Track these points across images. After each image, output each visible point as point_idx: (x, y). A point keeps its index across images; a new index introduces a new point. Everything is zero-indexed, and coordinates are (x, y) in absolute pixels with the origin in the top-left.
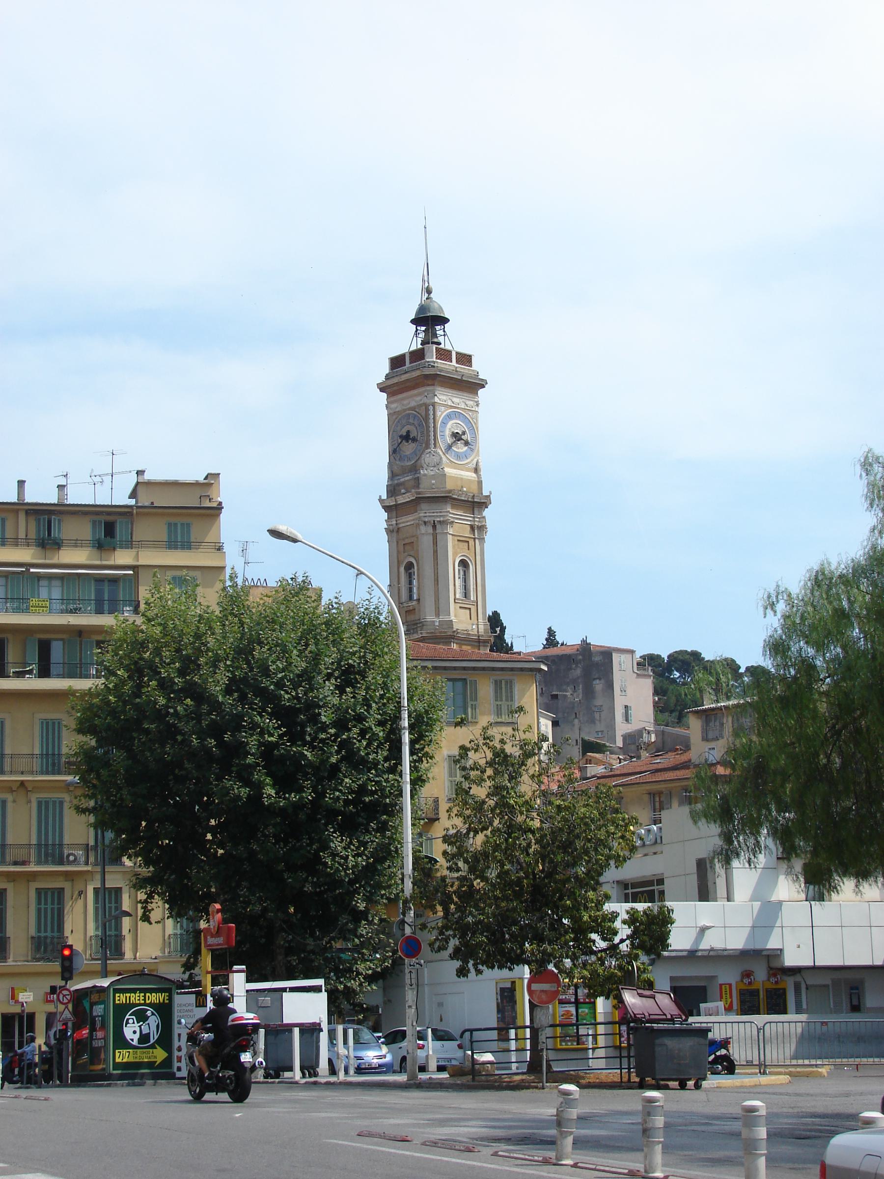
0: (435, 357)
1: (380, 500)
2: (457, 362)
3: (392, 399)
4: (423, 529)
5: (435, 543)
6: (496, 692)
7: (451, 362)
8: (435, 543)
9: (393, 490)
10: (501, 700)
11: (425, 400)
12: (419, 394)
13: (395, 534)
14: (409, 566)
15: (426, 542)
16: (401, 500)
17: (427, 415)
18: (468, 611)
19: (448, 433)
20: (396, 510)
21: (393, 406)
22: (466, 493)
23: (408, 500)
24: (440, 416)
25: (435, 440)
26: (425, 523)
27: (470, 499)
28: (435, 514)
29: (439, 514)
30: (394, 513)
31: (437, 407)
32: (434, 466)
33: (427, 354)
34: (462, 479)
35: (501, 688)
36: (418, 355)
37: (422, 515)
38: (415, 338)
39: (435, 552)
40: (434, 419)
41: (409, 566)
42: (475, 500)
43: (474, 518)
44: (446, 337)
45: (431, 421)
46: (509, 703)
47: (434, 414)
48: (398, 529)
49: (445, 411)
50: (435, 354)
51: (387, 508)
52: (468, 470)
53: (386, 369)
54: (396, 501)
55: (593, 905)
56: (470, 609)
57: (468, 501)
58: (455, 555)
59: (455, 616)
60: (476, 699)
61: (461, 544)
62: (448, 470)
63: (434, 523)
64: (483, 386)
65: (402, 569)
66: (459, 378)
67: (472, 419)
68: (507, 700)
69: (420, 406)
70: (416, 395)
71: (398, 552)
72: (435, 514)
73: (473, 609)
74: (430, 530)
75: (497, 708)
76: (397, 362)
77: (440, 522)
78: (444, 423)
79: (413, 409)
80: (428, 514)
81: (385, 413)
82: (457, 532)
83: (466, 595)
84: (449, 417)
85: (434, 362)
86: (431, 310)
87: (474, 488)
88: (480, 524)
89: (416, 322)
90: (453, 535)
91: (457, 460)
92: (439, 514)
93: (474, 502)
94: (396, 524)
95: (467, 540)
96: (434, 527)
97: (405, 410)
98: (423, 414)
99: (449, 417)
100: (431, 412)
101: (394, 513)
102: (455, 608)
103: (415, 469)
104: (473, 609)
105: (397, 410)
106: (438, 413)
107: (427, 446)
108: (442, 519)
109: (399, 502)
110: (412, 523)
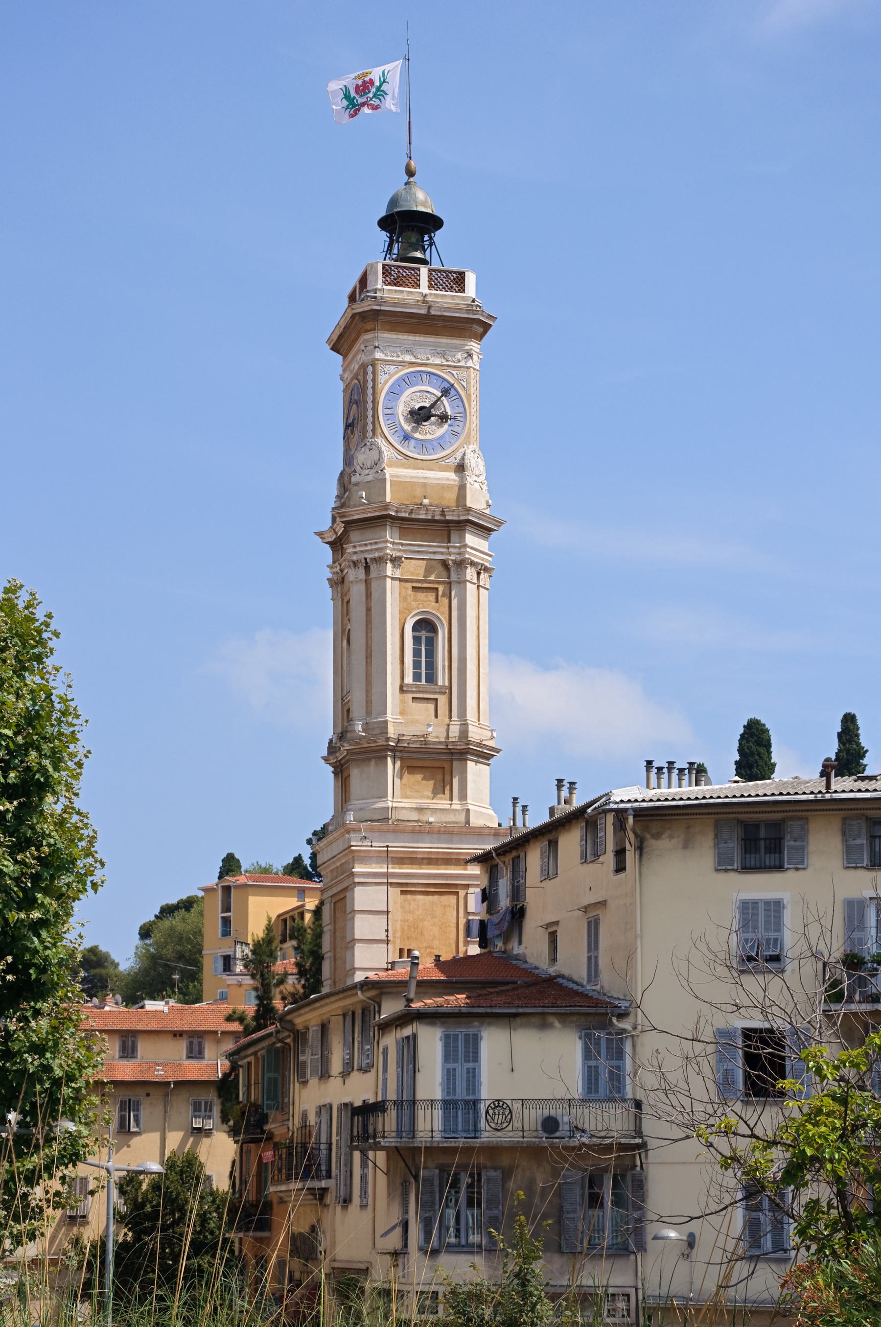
18: (431, 706)
19: (402, 410)
24: (386, 382)
25: (373, 423)
26: (355, 564)
27: (437, 518)
28: (369, 547)
29: (374, 547)
31: (379, 367)
34: (424, 485)
42: (448, 518)
43: (448, 548)
44: (433, 247)
45: (370, 391)
49: (396, 373)
56: (436, 700)
57: (433, 521)
61: (421, 596)
63: (366, 563)
66: (423, 312)
72: (369, 547)
73: (442, 700)
77: (375, 560)
78: (395, 393)
80: (358, 549)
83: (431, 678)
84: (406, 381)
87: (450, 498)
88: (459, 558)
89: (385, 223)
91: (422, 453)
92: (374, 547)
95: (436, 586)
96: (367, 568)
99: (406, 381)
100: (370, 377)
102: (403, 701)
104: (442, 700)
106: (382, 378)
108: (376, 555)
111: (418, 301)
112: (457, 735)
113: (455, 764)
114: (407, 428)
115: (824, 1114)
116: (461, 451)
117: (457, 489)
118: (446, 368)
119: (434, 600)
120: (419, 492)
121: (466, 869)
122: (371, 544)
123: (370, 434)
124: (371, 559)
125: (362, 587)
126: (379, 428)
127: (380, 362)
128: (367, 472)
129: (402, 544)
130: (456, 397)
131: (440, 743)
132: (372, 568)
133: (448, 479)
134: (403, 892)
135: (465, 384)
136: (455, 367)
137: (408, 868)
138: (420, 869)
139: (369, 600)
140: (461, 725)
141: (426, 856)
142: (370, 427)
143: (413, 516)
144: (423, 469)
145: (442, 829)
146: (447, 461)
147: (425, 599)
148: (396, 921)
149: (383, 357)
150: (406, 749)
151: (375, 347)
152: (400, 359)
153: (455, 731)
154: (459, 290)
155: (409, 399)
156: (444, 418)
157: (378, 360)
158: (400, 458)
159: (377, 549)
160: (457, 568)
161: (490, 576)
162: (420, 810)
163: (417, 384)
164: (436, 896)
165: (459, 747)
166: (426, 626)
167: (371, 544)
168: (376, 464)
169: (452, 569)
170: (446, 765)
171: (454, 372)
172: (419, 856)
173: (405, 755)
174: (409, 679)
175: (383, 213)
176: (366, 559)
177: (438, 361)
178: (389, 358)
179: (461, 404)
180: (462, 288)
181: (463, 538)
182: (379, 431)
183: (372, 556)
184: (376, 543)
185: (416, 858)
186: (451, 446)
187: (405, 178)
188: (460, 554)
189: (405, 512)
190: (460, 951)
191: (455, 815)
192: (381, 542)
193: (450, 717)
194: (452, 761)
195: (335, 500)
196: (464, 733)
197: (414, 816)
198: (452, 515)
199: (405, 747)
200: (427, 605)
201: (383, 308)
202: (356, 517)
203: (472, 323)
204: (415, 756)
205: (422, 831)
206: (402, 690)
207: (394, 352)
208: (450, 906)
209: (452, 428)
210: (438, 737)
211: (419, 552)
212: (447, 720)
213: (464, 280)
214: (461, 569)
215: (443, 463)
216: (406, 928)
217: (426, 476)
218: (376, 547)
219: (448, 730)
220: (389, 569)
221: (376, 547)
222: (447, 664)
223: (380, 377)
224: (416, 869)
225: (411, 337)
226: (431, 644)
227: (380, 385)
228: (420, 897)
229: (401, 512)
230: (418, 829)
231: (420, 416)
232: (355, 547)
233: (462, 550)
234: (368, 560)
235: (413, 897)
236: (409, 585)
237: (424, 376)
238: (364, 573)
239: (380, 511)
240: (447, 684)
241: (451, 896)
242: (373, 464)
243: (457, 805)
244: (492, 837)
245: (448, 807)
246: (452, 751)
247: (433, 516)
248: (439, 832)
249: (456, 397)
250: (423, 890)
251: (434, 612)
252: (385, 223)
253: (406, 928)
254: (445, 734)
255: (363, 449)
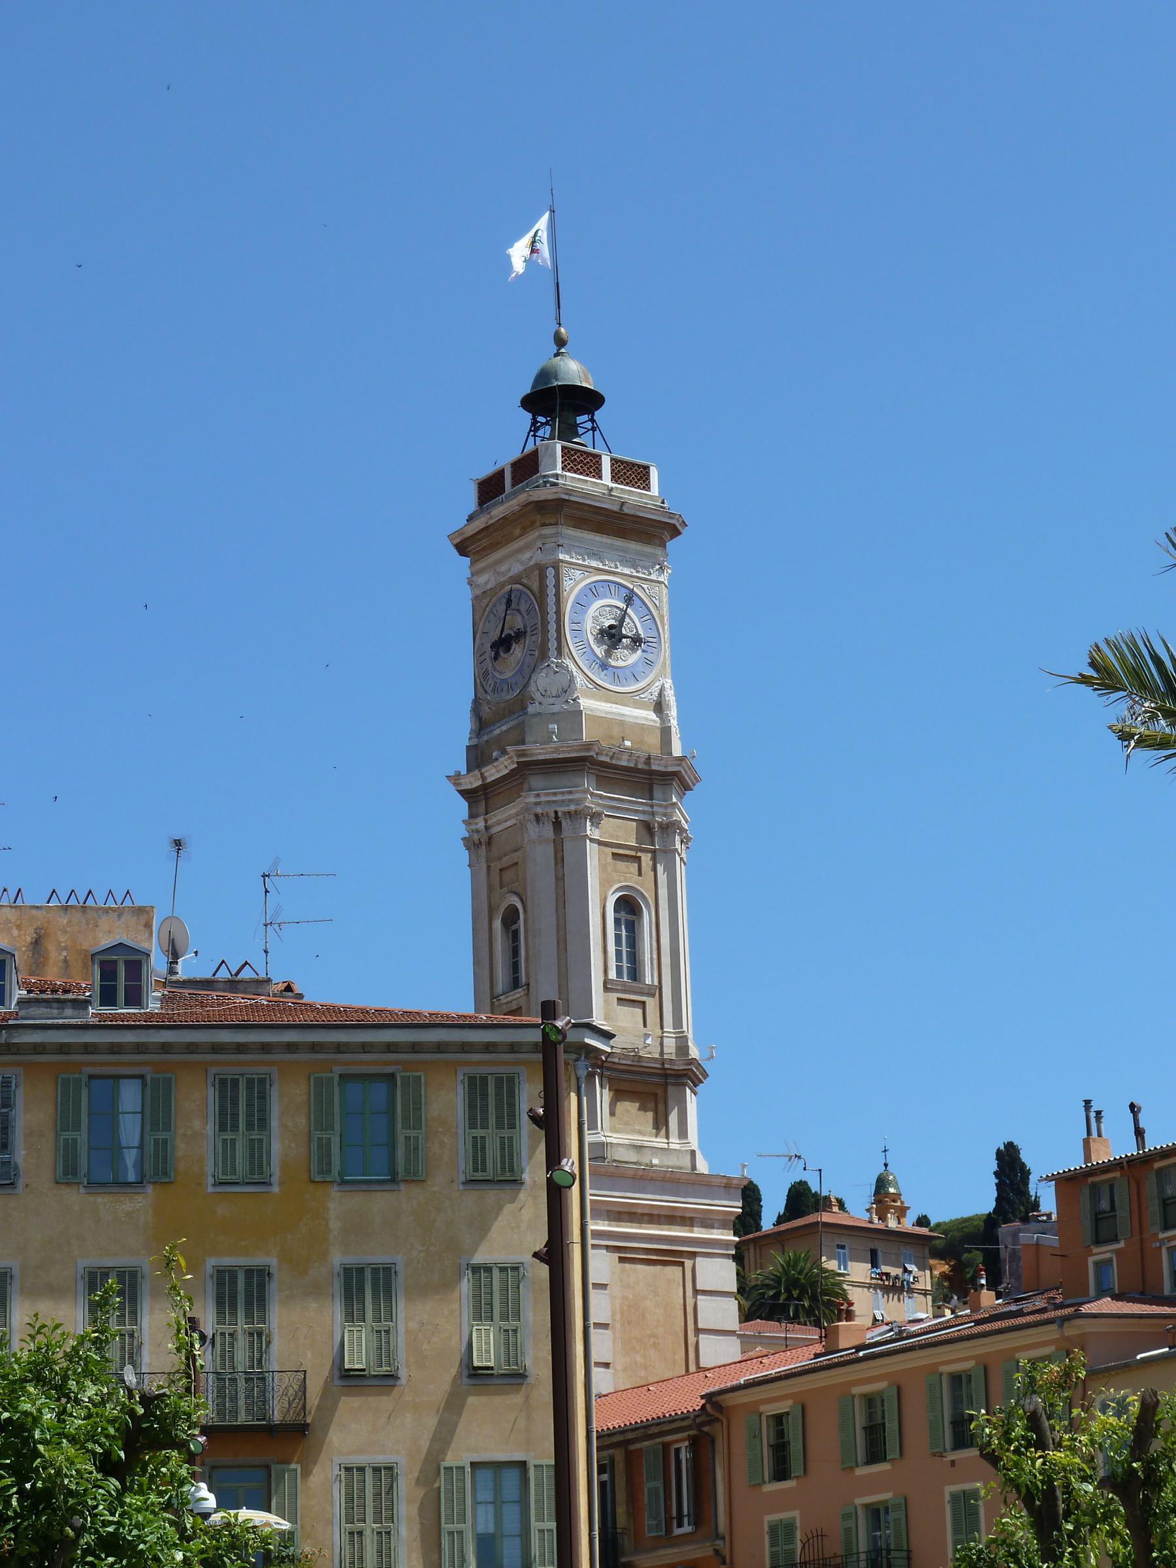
0: (559, 465)
1: (455, 779)
2: (615, 478)
3: (480, 565)
4: (533, 830)
5: (559, 859)
6: (472, 1106)
7: (600, 478)
8: (559, 859)
9: (477, 757)
10: (485, 1126)
11: (539, 557)
12: (528, 547)
13: (483, 850)
14: (511, 917)
15: (540, 856)
16: (493, 773)
17: (543, 587)
19: (590, 627)
20: (486, 799)
21: (482, 579)
22: (630, 752)
23: (505, 772)
24: (572, 589)
26: (537, 817)
27: (640, 766)
28: (559, 798)
30: (482, 808)
31: (564, 570)
32: (557, 696)
33: (543, 461)
35: (485, 1096)
36: (527, 466)
37: (532, 799)
38: (531, 439)
39: (560, 879)
40: (558, 595)
41: (511, 917)
42: (654, 767)
43: (652, 806)
44: (597, 433)
45: (551, 600)
46: (506, 1133)
47: (557, 586)
48: (490, 838)
49: (582, 580)
50: (559, 459)
51: (465, 794)
52: (640, 705)
53: (470, 501)
54: (483, 778)
55: (224, 1539)
56: (644, 1003)
57: (635, 770)
58: (605, 884)
59: (606, 1019)
60: (417, 1125)
61: (621, 865)
62: (585, 703)
63: (557, 817)
64: (675, 532)
65: (498, 924)
67: (650, 597)
68: (500, 1125)
69: (528, 571)
70: (520, 550)
71: (490, 889)
73: (651, 1003)
74: (548, 831)
75: (475, 1145)
76: (490, 489)
79: (517, 579)
80: (543, 799)
81: (467, 594)
82: (611, 836)
83: (635, 973)
84: (593, 591)
85: (557, 476)
86: (561, 375)
87: (653, 743)
89: (529, 403)
90: (600, 843)
91: (613, 683)
93: (652, 773)
94: (487, 828)
96: (557, 825)
97: (503, 585)
98: (535, 586)
99: (593, 591)
100: (550, 581)
101: (482, 808)
102: (606, 1002)
103: (520, 704)
105: (489, 587)
106: (567, 584)
107: (544, 655)
108: (572, 808)
109: (489, 780)
110: (513, 821)
111: (604, 494)
112: (674, 1051)
113: (671, 1089)
114: (600, 651)
115: (25, 1380)
116: (656, 684)
117: (658, 732)
118: (636, 580)
119: (637, 873)
120: (616, 732)
121: (692, 1232)
122: (563, 793)
123: (553, 652)
124: (564, 813)
125: (550, 849)
126: (566, 647)
127: (564, 565)
128: (552, 700)
129: (601, 797)
130: (648, 617)
131: (655, 1060)
132: (564, 824)
133: (646, 719)
134: (622, 1260)
135: (657, 602)
136: (646, 580)
137: (675, 1231)
138: (640, 1228)
139: (559, 866)
140: (676, 1038)
141: (646, 1212)
142: (552, 645)
143: (614, 762)
144: (616, 703)
145: (668, 1175)
146: (642, 696)
147: (626, 870)
148: (615, 1298)
149: (567, 558)
150: (614, 1066)
151: (559, 545)
152: (586, 563)
153: (670, 1045)
154: (644, 487)
155: (598, 614)
156: (637, 641)
157: (562, 561)
158: (591, 687)
159: (571, 801)
160: (662, 833)
161: (687, 848)
162: (639, 1148)
163: (605, 597)
164: (659, 1267)
165: (676, 1068)
166: (628, 906)
167: (563, 793)
168: (566, 692)
169: (656, 834)
170: (660, 1092)
171: (645, 586)
172: (640, 1211)
173: (614, 1074)
174: (613, 975)
175: (527, 389)
176: (556, 812)
177: (627, 571)
178: (574, 560)
179: (655, 627)
180: (647, 485)
181: (667, 798)
182: (566, 650)
183: (566, 809)
184: (570, 792)
185: (635, 1213)
186: (646, 677)
187: (554, 349)
188: (665, 815)
189: (607, 755)
190: (689, 1342)
191: (678, 1157)
192: (577, 792)
193: (662, 1027)
194: (666, 1085)
195: (469, 736)
196: (682, 1048)
197: (632, 1156)
198: (659, 765)
199: (614, 1063)
200: (626, 875)
201: (572, 498)
202: (542, 757)
203: (663, 529)
204: (625, 1076)
205: (644, 1178)
206: (606, 989)
207: (580, 555)
208: (674, 1281)
209: (645, 655)
210: (650, 1053)
211: (618, 808)
212: (659, 1032)
213: (649, 475)
214: (668, 835)
215: (638, 698)
216: (625, 1309)
217: (622, 712)
218: (571, 797)
219: (662, 1044)
220: (590, 830)
221: (571, 797)
222: (655, 956)
223: (565, 583)
224: (636, 1228)
225: (597, 538)
226: (633, 929)
227: (565, 593)
228: (640, 1267)
229: (602, 754)
230: (640, 1173)
231: (612, 636)
232: (538, 795)
233: (669, 810)
234: (560, 814)
235: (632, 1266)
236: (609, 850)
237: (612, 588)
238: (552, 830)
239: (577, 751)
240: (656, 983)
241: (675, 1268)
242: (560, 690)
243: (675, 1143)
244: (722, 1190)
245: (666, 1146)
246: (668, 1072)
247: (637, 763)
248: (668, 1181)
249: (648, 617)
250: (655, 1258)
251: (639, 888)
252: (529, 403)
253: (625, 1309)
254: (659, 1049)
255: (544, 671)
